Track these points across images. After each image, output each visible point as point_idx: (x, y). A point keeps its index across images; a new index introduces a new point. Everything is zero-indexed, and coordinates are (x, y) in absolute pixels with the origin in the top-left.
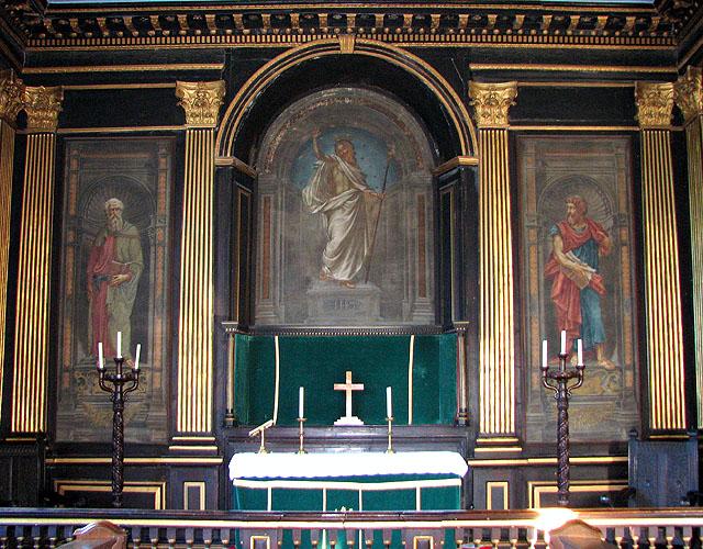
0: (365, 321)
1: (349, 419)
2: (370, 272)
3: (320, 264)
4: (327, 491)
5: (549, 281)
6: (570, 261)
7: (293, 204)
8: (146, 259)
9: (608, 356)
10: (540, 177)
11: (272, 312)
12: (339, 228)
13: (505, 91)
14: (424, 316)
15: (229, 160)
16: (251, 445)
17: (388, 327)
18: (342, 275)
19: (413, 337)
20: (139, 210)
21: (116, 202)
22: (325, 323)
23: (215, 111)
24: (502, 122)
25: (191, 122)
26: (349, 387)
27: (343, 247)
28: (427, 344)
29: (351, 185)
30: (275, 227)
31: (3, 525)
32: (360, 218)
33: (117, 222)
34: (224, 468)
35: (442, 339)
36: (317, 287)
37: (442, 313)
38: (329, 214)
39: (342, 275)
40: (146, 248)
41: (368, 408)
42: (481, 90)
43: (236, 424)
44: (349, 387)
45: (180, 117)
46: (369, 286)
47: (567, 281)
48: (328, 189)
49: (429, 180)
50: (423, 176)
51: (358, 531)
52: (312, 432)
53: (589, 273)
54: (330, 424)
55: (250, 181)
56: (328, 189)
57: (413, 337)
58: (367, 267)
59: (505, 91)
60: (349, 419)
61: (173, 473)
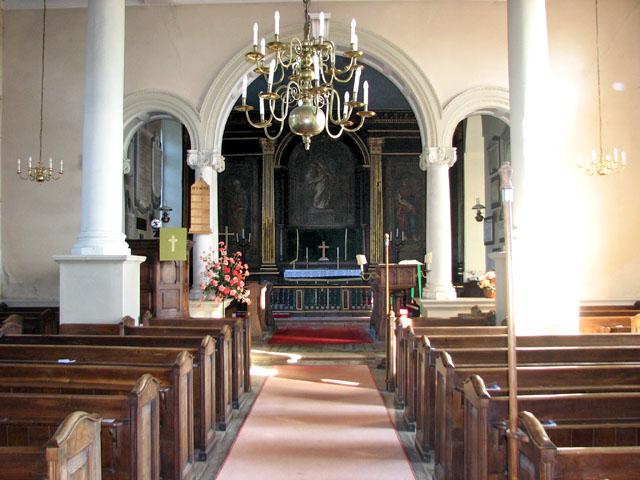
0: (329, 224)
1: (324, 259)
2: (331, 205)
3: (312, 202)
4: (507, 352)
5: (396, 211)
6: (404, 203)
7: (302, 180)
8: (249, 202)
9: (417, 237)
10: (393, 172)
11: (296, 220)
12: (319, 189)
13: (380, 141)
14: (351, 221)
15: (279, 166)
16: (291, 267)
17: (337, 226)
18: (321, 206)
19: (173, 250)
20: (246, 185)
21: (237, 182)
22: (313, 225)
23: (273, 149)
24: (379, 152)
25: (265, 153)
26: (324, 247)
27: (321, 195)
28: (352, 231)
29: (323, 173)
30: (296, 189)
31: (1, 368)
32: (327, 184)
33: (238, 189)
34: (282, 275)
35: (358, 231)
36: (312, 211)
37: (357, 222)
38: (316, 184)
39: (321, 206)
40: (249, 198)
41: (330, 254)
42: (372, 140)
43: (284, 261)
44: (324, 247)
45: (261, 151)
46: (331, 210)
47: (402, 210)
48: (316, 174)
49: (353, 171)
50: (351, 169)
51: (508, 395)
52: (311, 263)
53: (410, 206)
54: (317, 260)
55: (286, 172)
56: (316, 174)
57: (173, 250)
58: (330, 203)
59: (380, 141)
60: (324, 259)
61: (262, 278)
